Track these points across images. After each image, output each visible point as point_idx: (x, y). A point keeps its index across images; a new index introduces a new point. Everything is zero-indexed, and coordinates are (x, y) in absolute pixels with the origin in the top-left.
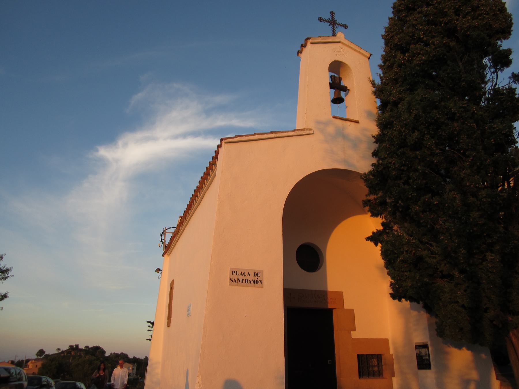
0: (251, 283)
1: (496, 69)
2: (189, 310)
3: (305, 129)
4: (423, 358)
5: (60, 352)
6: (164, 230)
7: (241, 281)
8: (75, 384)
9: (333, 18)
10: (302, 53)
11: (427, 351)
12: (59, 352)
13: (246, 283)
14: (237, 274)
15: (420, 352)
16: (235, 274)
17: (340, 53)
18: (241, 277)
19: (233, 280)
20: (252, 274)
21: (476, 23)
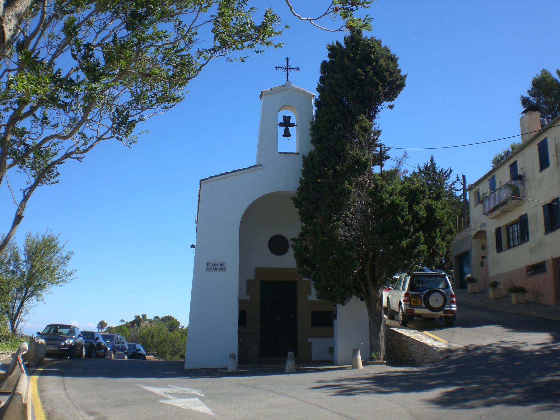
5: (124, 323)
8: (135, 346)
12: (123, 324)
18: (212, 267)
20: (219, 265)
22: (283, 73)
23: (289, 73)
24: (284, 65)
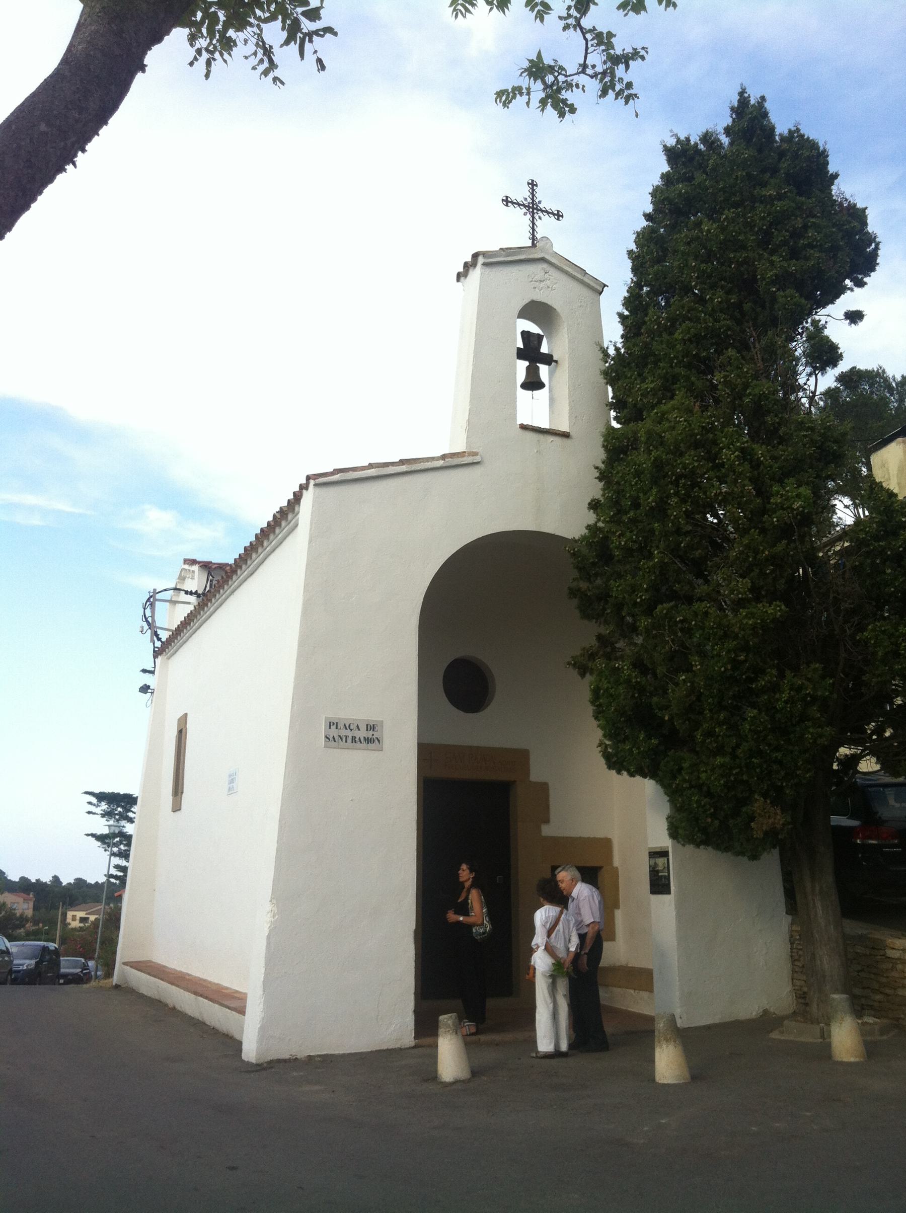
0: (361, 743)
1: (815, 368)
2: (232, 781)
3: (465, 452)
4: (660, 874)
6: (151, 594)
7: (344, 740)
9: (533, 195)
10: (468, 278)
11: (666, 862)
13: (352, 742)
14: (337, 728)
15: (655, 863)
16: (334, 727)
17: (542, 285)
18: (344, 733)
19: (331, 738)
20: (363, 728)
21: (794, 268)
22: (521, 218)
23: (538, 222)
24: (540, 218)
